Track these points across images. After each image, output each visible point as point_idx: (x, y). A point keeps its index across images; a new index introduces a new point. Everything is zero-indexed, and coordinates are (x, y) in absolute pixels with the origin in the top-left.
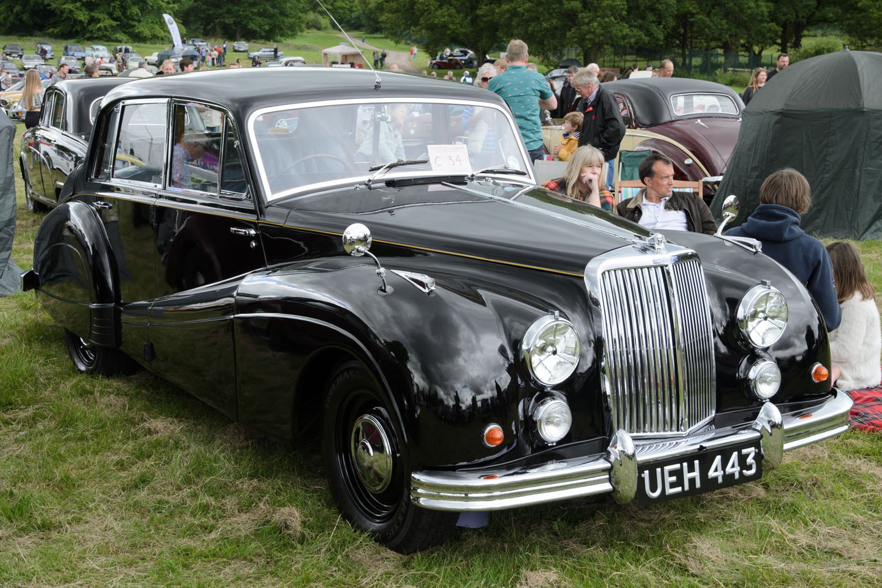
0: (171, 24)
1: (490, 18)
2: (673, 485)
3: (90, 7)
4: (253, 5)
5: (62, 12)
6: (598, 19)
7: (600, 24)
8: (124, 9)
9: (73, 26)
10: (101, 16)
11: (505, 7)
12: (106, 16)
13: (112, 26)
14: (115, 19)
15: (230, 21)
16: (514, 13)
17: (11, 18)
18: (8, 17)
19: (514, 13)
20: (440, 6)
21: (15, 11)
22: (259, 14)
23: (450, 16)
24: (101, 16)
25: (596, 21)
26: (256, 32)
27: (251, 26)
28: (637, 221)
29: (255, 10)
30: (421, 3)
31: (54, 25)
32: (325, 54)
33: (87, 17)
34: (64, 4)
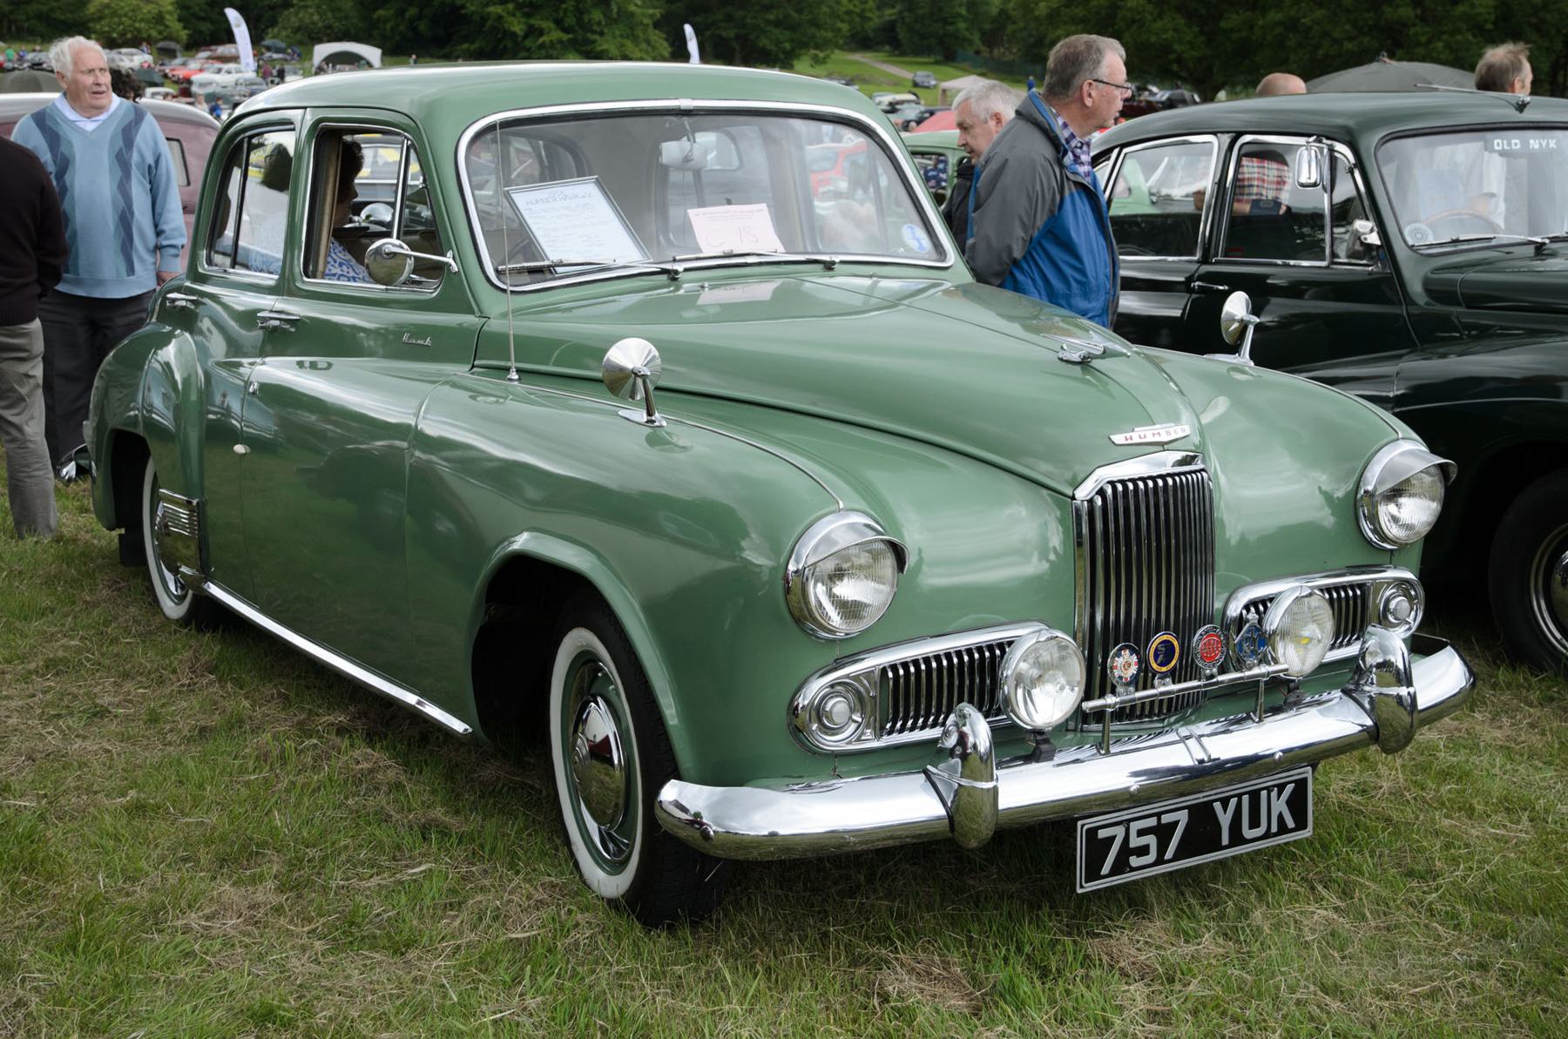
1: (1244, 34)
3: (530, 10)
4: (768, 8)
5: (484, 19)
6: (1445, 37)
7: (1448, 46)
8: (580, 12)
10: (545, 25)
11: (1275, 16)
12: (552, 25)
13: (560, 41)
14: (565, 31)
15: (730, 33)
16: (1292, 25)
17: (402, 28)
19: (1292, 25)
20: (1160, 16)
21: (407, 15)
22: (777, 23)
23: (1176, 30)
24: (545, 25)
27: (764, 42)
28: (1123, 289)
29: (771, 17)
30: (1130, 9)
31: (466, 39)
32: (944, 91)
33: (523, 27)
34: (487, 5)
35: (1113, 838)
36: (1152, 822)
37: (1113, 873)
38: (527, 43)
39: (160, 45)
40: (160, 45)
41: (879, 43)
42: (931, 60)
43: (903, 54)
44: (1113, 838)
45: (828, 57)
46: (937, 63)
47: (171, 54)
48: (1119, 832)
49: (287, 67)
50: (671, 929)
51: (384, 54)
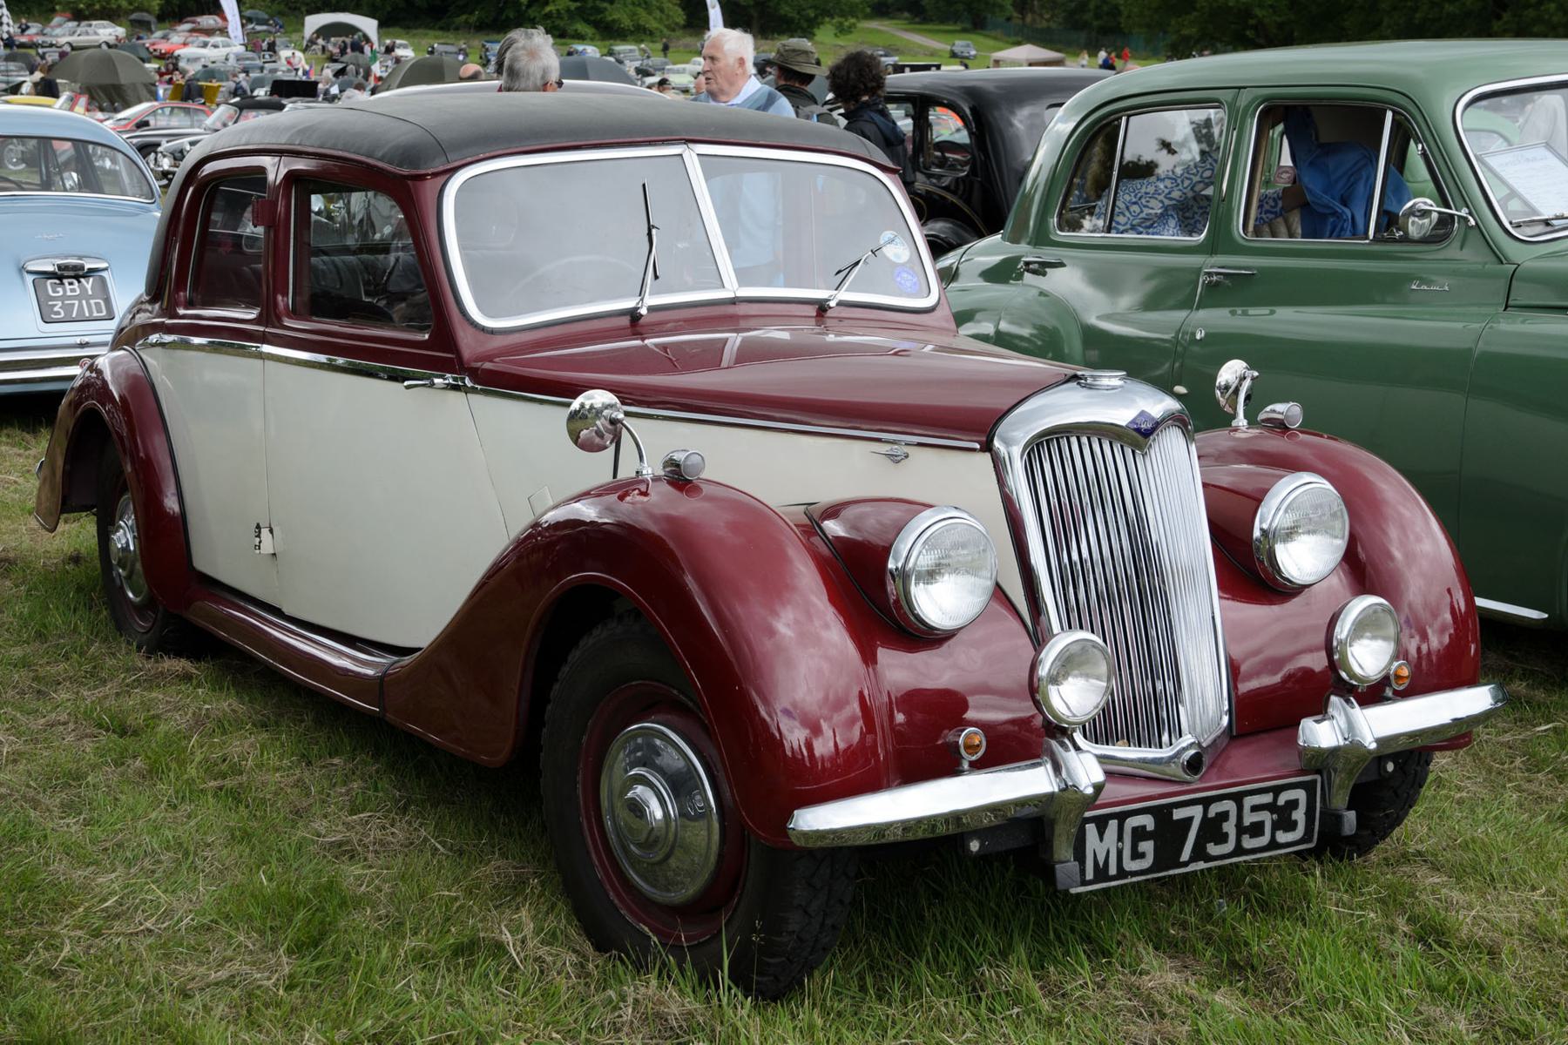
13: (568, 10)
31: (464, 9)
35: (1190, 819)
36: (1267, 798)
37: (1193, 859)
38: (532, 12)
39: (134, 16)
40: (134, 16)
41: (900, 10)
42: (958, 27)
43: (925, 20)
44: (1190, 819)
45: (853, 26)
46: (964, 31)
47: (145, 26)
48: (1196, 812)
49: (278, 41)
50: (1099, 952)
51: (381, 26)
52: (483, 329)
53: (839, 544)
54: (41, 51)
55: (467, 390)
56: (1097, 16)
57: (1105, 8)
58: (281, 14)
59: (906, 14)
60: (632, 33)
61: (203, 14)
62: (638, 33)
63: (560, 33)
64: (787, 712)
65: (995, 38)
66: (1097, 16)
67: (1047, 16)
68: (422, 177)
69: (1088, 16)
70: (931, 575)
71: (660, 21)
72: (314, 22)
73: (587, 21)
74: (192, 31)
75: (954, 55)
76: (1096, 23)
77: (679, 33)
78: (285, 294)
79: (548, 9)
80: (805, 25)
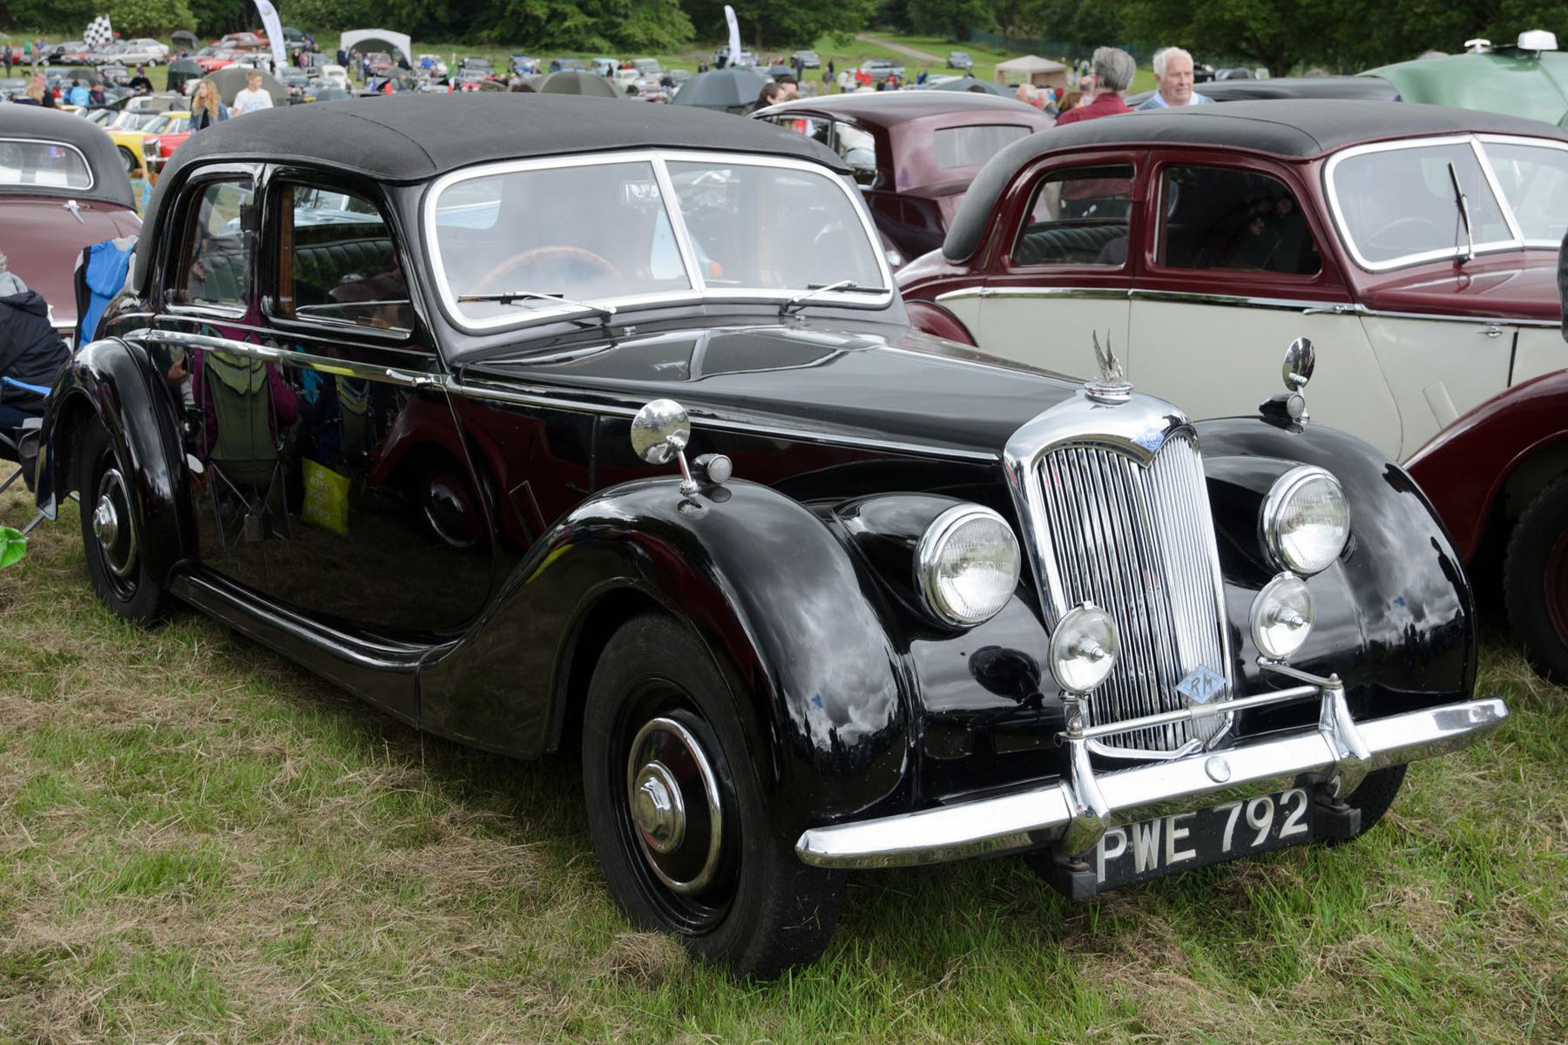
0: (268, 14)
1: (1322, 9)
2: (1181, 845)
6: (1539, 10)
9: (521, 26)
12: (576, 10)
13: (586, 26)
14: (590, 14)
17: (419, 14)
18: (414, 11)
25: (1532, 13)
26: (794, 32)
27: (787, 22)
31: (485, 25)
32: (1001, 72)
33: (546, 10)
39: (177, 34)
40: (177, 34)
41: (886, 23)
46: (950, 42)
51: (413, 41)
52: (1366, 271)
53: (864, 539)
54: (99, 68)
55: (1360, 314)
56: (1082, 28)
57: (1090, 20)
58: (310, 30)
59: (891, 28)
60: (646, 46)
61: (244, 30)
62: (653, 46)
63: (1200, 53)
64: (931, 682)
65: (981, 50)
66: (1082, 28)
67: (1026, 28)
68: (1306, 162)
69: (1071, 28)
70: (955, 569)
71: (672, 35)
72: (350, 38)
73: (604, 36)
74: (237, 47)
75: (951, 66)
76: (1081, 35)
77: (690, 46)
78: (1151, 251)
79: (567, 24)
80: (806, 38)
